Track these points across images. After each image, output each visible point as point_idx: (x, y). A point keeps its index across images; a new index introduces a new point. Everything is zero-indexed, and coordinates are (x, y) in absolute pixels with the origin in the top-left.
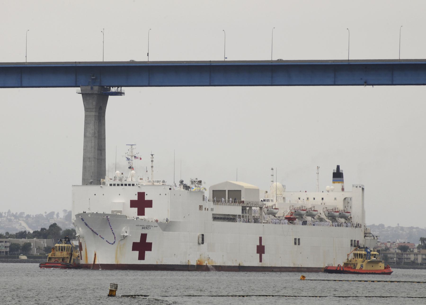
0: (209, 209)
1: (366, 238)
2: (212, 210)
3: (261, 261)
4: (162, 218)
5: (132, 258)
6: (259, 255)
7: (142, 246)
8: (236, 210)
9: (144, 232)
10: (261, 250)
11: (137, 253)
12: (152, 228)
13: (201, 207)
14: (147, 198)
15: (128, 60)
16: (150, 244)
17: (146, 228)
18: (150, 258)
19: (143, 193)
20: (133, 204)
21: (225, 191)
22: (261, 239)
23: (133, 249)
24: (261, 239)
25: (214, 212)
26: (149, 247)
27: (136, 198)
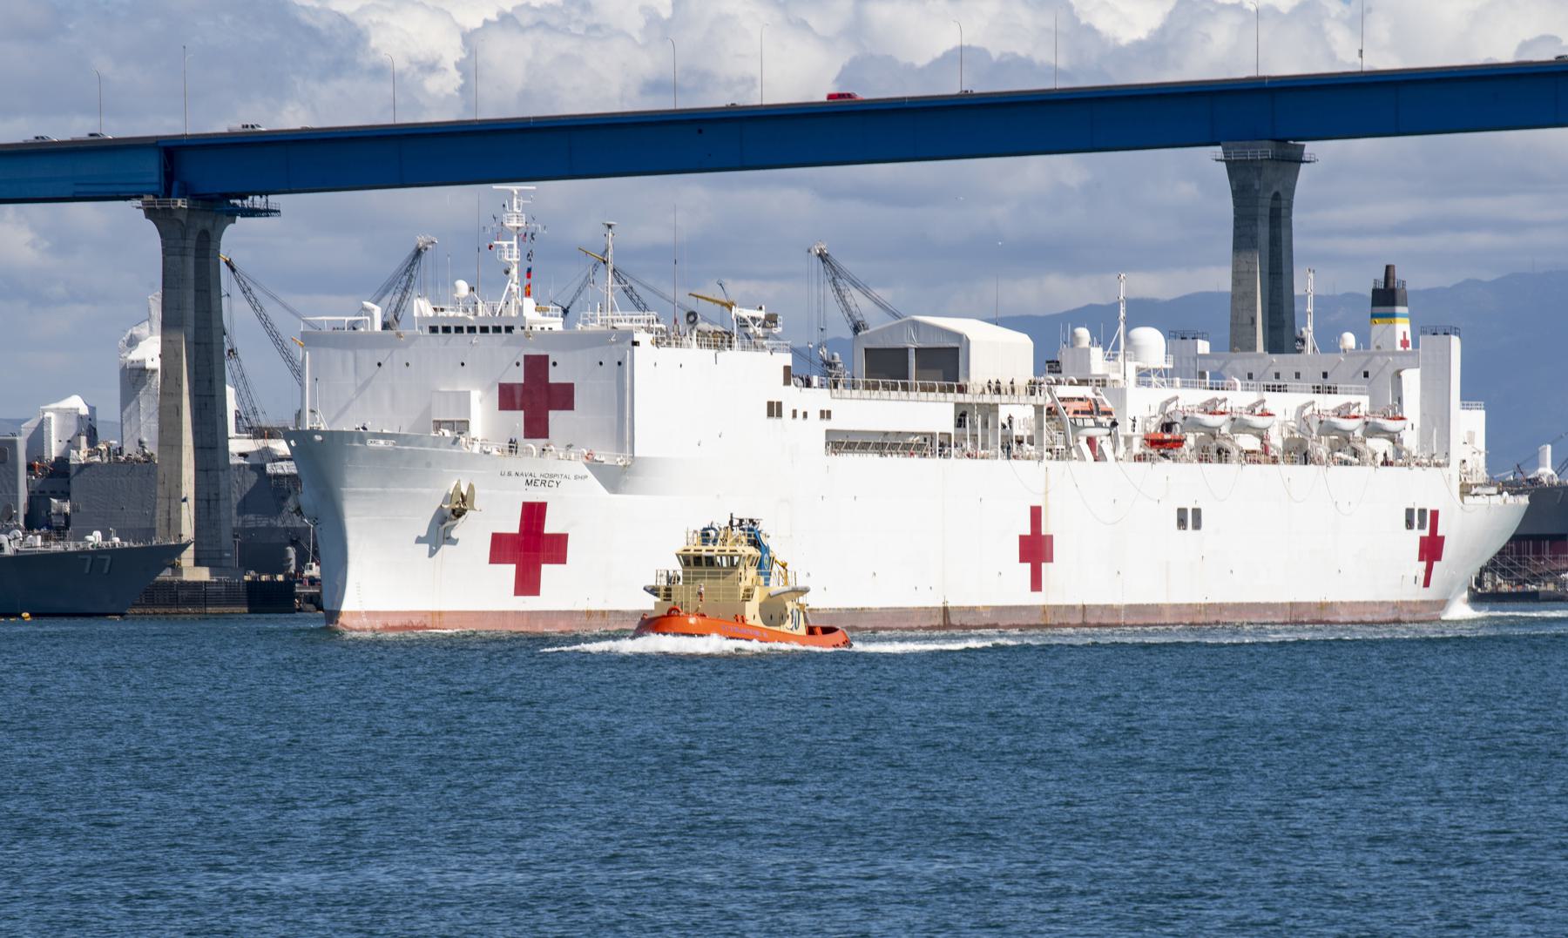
0: (814, 415)
1: (1468, 499)
2: (825, 415)
3: (1036, 584)
6: (1439, 533)
9: (535, 496)
10: (1035, 549)
11: (509, 571)
12: (564, 482)
13: (774, 409)
16: (560, 541)
17: (544, 483)
19: (544, 360)
21: (906, 350)
22: (1036, 513)
23: (494, 559)
24: (1036, 513)
25: (835, 424)
26: (556, 549)
27: (517, 376)
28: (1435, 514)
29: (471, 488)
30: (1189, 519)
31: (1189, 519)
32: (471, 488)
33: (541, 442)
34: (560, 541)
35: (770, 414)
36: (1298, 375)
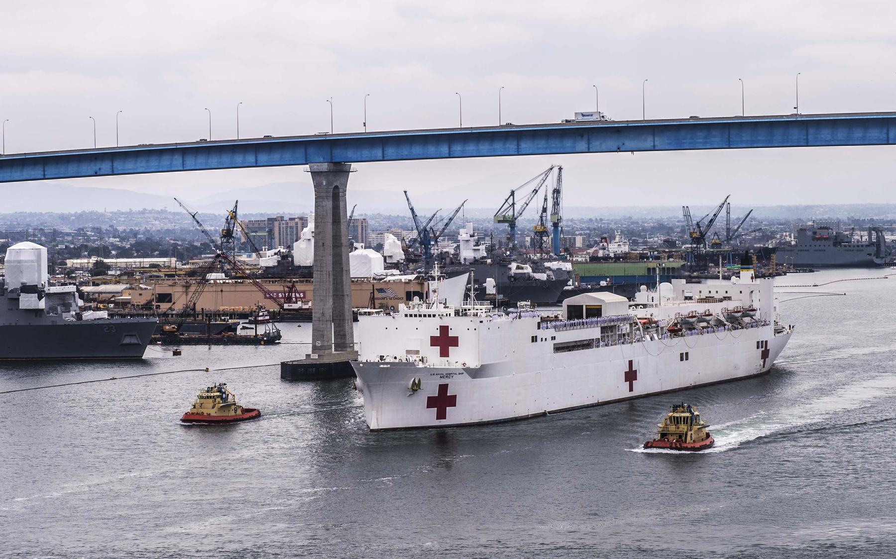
0: (549, 339)
2: (553, 338)
3: (631, 389)
4: (473, 364)
5: (429, 418)
7: (442, 401)
8: (594, 333)
9: (444, 381)
10: (631, 376)
13: (534, 339)
14: (451, 334)
15: (11, 211)
16: (454, 398)
18: (454, 416)
20: (434, 341)
22: (631, 362)
24: (631, 362)
26: (452, 401)
27: (437, 334)
28: (766, 342)
29: (419, 381)
30: (684, 357)
31: (684, 357)
32: (419, 381)
33: (446, 359)
34: (454, 398)
35: (533, 341)
36: (481, 322)
